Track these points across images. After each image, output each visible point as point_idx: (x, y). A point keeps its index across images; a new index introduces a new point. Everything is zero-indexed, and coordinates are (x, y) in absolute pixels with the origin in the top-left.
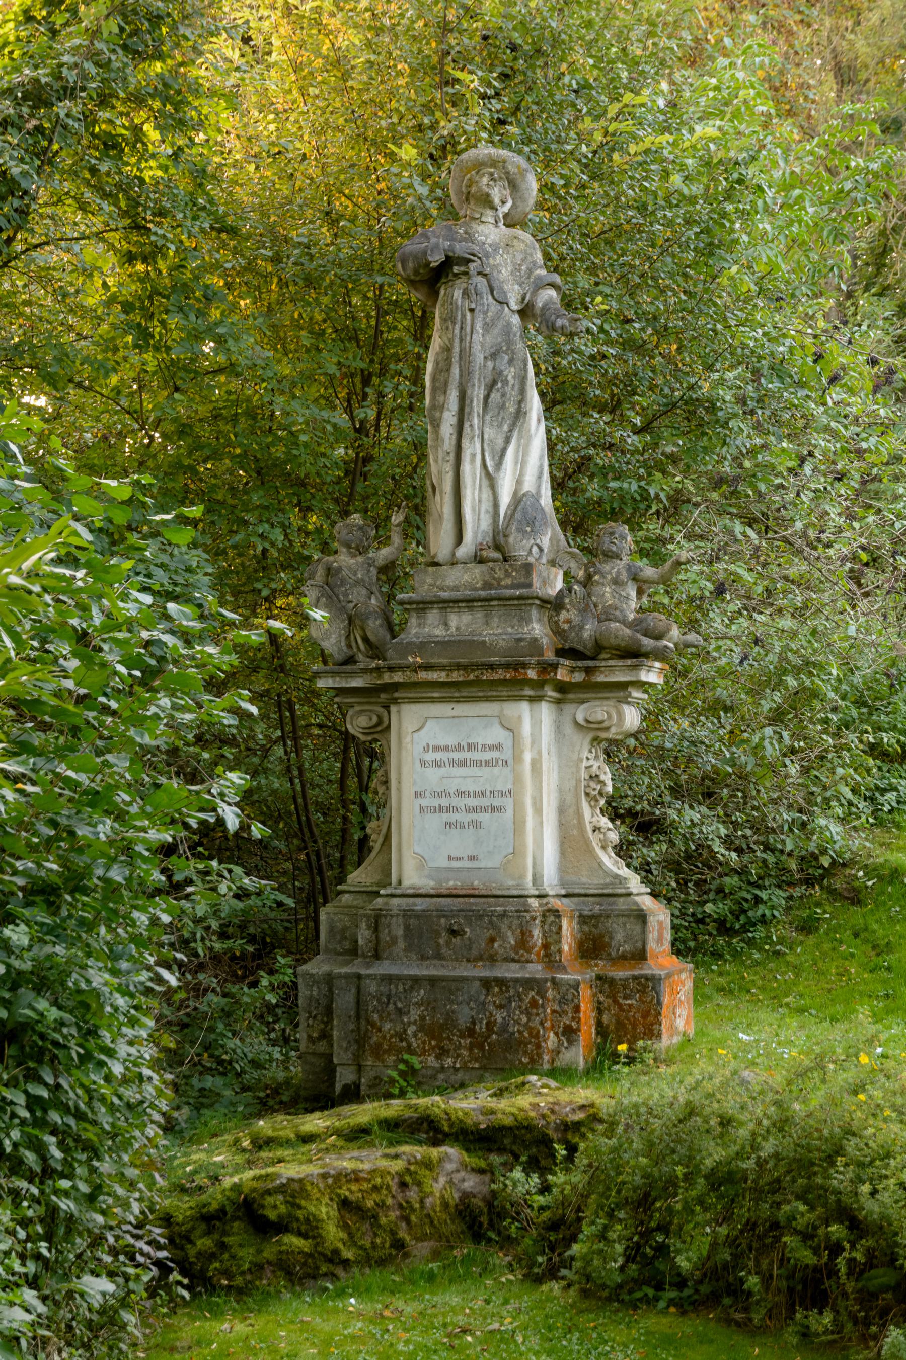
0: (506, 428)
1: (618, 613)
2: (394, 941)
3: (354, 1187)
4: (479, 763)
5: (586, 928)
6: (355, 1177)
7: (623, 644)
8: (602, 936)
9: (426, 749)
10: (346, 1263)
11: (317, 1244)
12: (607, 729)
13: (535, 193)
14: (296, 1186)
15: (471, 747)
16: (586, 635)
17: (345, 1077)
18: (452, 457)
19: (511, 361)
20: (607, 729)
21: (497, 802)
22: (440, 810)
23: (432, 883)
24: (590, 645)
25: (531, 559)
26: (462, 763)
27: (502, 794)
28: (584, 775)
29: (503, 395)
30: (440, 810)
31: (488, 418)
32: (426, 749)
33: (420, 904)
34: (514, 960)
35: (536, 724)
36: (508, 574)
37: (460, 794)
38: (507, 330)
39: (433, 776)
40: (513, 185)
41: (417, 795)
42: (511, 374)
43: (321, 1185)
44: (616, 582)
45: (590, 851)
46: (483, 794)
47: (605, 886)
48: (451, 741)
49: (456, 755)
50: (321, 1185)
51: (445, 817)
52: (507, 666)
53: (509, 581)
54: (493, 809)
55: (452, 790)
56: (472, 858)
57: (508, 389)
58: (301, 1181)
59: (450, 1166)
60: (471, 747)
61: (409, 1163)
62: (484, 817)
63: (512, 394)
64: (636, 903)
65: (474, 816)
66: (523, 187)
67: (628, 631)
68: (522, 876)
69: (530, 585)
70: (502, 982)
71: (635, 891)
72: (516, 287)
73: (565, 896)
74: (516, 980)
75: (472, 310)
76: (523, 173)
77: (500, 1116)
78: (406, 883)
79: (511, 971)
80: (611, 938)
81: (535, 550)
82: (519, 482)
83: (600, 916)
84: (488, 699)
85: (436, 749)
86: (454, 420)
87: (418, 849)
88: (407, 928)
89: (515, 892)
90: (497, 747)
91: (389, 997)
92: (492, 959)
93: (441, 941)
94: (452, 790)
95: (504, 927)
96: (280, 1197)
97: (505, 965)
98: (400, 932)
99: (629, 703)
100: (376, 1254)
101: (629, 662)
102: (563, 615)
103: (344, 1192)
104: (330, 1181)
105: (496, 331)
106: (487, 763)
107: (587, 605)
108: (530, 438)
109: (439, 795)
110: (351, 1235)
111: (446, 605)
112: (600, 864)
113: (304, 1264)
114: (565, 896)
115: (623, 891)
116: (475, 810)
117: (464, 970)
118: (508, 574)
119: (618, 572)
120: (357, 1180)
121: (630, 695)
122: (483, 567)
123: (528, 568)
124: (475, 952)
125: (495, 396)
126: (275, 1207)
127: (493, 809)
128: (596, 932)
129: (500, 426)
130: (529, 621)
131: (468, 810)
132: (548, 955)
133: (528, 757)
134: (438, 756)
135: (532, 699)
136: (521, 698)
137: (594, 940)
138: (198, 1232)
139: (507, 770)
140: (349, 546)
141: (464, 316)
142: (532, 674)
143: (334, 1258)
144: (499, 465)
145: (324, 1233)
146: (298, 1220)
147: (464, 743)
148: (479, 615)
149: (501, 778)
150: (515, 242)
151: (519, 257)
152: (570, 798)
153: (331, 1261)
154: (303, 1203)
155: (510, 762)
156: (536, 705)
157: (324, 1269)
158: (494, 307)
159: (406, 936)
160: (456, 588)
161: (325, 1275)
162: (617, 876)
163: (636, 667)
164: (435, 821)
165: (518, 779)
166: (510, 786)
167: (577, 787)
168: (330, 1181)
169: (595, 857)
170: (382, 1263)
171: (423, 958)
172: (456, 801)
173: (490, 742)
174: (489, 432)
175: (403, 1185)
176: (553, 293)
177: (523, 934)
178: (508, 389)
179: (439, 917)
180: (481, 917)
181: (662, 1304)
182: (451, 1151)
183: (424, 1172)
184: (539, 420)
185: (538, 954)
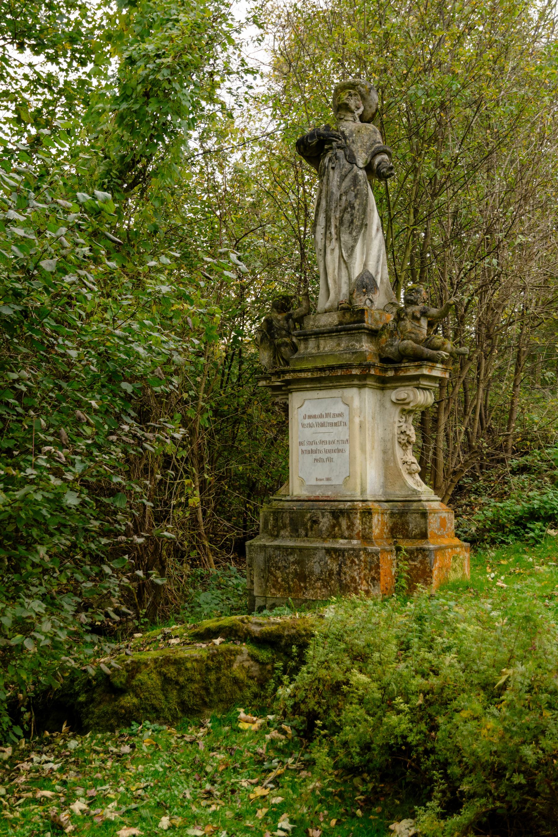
1: (413, 335)
4: (331, 425)
12: (408, 404)
15: (328, 415)
17: (259, 602)
18: (322, 253)
20: (408, 404)
22: (312, 452)
23: (310, 495)
25: (365, 307)
26: (323, 425)
27: (343, 442)
28: (396, 431)
29: (352, 215)
30: (312, 452)
32: (305, 418)
37: (322, 442)
39: (308, 432)
41: (301, 444)
45: (400, 475)
47: (408, 496)
48: (317, 413)
49: (320, 420)
51: (314, 456)
54: (339, 451)
56: (328, 479)
60: (328, 415)
62: (334, 455)
64: (423, 506)
65: (328, 455)
66: (369, 98)
68: (355, 490)
69: (364, 322)
70: (336, 550)
71: (423, 498)
75: (333, 168)
78: (295, 494)
79: (341, 543)
81: (368, 301)
82: (365, 265)
84: (335, 387)
85: (310, 417)
86: (323, 231)
90: (340, 415)
101: (416, 363)
105: (347, 180)
106: (336, 424)
109: (311, 443)
111: (318, 334)
112: (405, 483)
114: (387, 501)
115: (417, 499)
127: (339, 451)
131: (326, 452)
133: (357, 420)
134: (310, 421)
135: (361, 387)
136: (352, 386)
139: (346, 428)
141: (328, 172)
142: (355, 372)
144: (350, 255)
152: (389, 445)
155: (347, 423)
160: (325, 326)
162: (414, 490)
164: (310, 458)
165: (351, 434)
167: (393, 438)
172: (320, 447)
182: (245, 648)
184: (378, 230)
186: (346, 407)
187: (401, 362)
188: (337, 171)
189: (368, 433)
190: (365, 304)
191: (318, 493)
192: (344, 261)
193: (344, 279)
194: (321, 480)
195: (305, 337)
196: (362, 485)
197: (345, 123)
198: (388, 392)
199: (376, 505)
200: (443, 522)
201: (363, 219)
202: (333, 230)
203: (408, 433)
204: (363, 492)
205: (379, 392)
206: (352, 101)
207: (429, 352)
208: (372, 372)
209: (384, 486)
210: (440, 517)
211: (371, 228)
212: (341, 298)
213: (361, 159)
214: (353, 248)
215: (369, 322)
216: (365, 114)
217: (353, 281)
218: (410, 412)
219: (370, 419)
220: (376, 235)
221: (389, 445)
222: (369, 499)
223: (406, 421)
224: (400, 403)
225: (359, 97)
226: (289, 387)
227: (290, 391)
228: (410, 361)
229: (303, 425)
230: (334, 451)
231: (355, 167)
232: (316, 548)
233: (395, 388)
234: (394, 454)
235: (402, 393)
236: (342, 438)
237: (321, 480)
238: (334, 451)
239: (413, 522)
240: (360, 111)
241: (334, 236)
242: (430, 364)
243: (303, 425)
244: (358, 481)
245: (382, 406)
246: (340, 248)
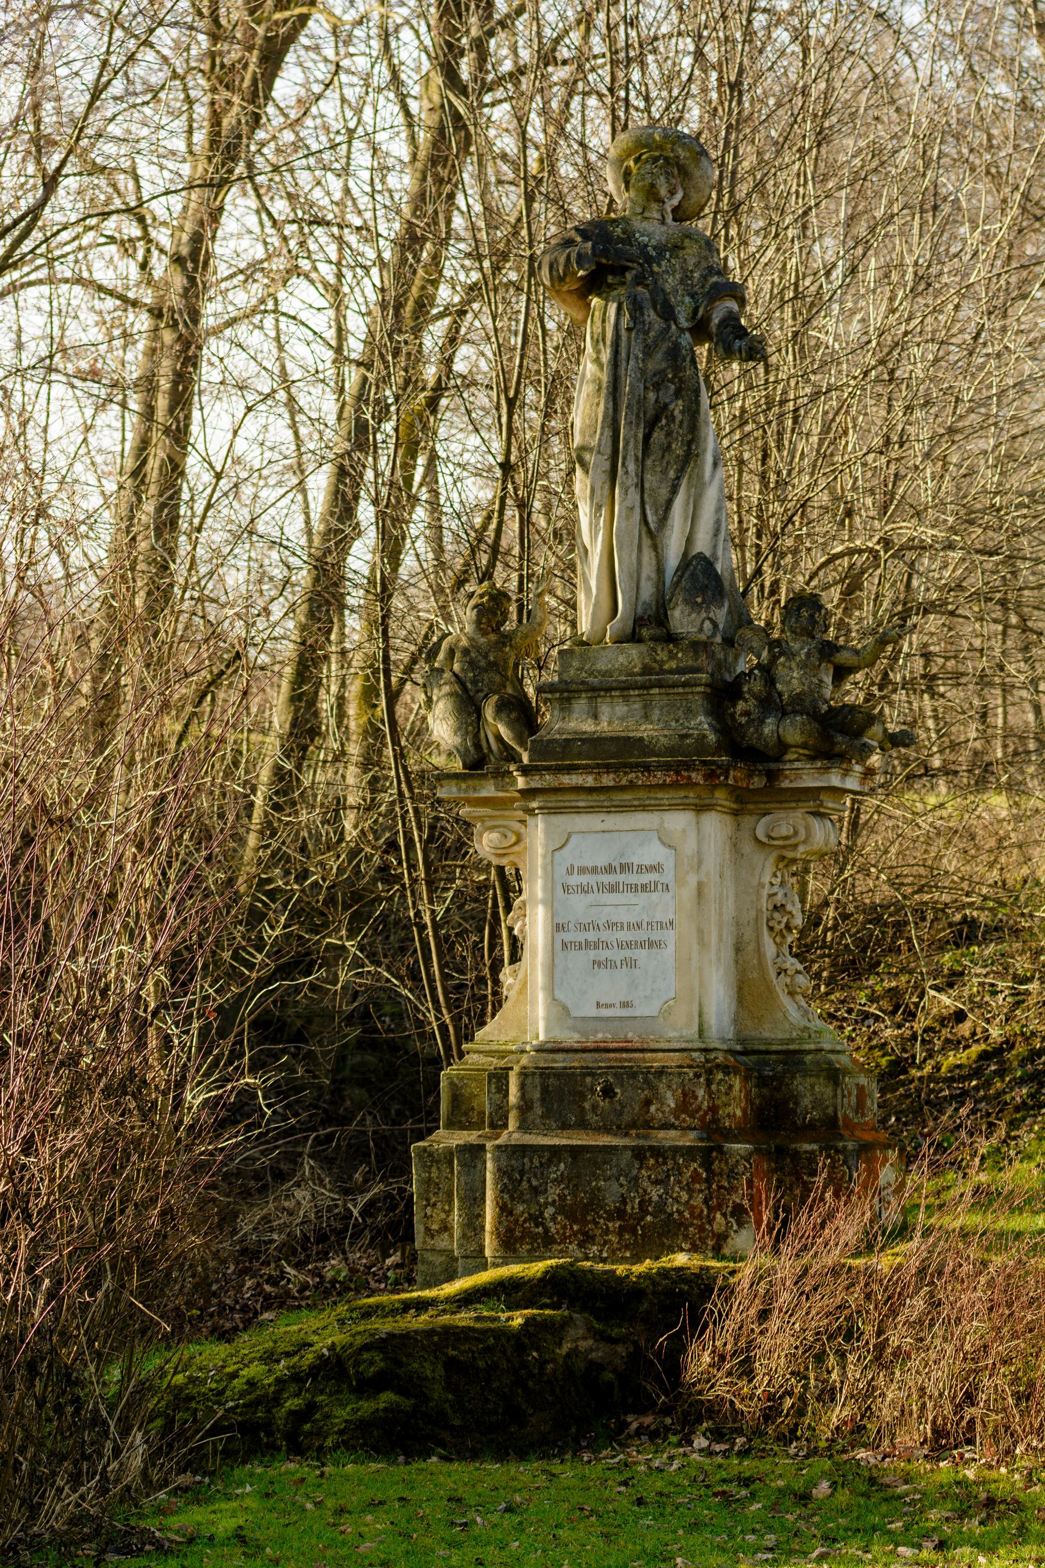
0: (672, 474)
5: (765, 1091)
9: (570, 871)
15: (625, 868)
21: (655, 936)
23: (576, 1037)
26: (613, 888)
27: (662, 926)
28: (765, 904)
29: (669, 434)
31: (649, 462)
32: (570, 871)
37: (611, 925)
42: (677, 408)
46: (639, 926)
48: (601, 862)
49: (607, 879)
51: (592, 954)
54: (651, 944)
56: (625, 1005)
57: (675, 427)
60: (625, 868)
65: (627, 953)
66: (697, 173)
80: (797, 1104)
82: (689, 541)
84: (644, 808)
85: (583, 870)
92: (648, 1125)
95: (662, 1087)
106: (644, 888)
109: (585, 928)
115: (812, 1047)
116: (629, 945)
124: (626, 1118)
125: (658, 436)
127: (651, 944)
131: (620, 946)
134: (584, 879)
139: (668, 896)
144: (664, 519)
147: (615, 864)
152: (748, 934)
159: (543, 1100)
166: (671, 917)
173: (647, 862)
178: (675, 427)
186: (667, 851)
190: (701, 630)
192: (649, 531)
193: (648, 569)
194: (608, 1006)
201: (689, 444)
205: (728, 818)
209: (736, 1021)
211: (703, 463)
214: (669, 503)
216: (685, 205)
221: (748, 934)
229: (566, 888)
234: (759, 950)
236: (658, 917)
237: (608, 1006)
240: (675, 202)
243: (566, 888)
245: (735, 846)
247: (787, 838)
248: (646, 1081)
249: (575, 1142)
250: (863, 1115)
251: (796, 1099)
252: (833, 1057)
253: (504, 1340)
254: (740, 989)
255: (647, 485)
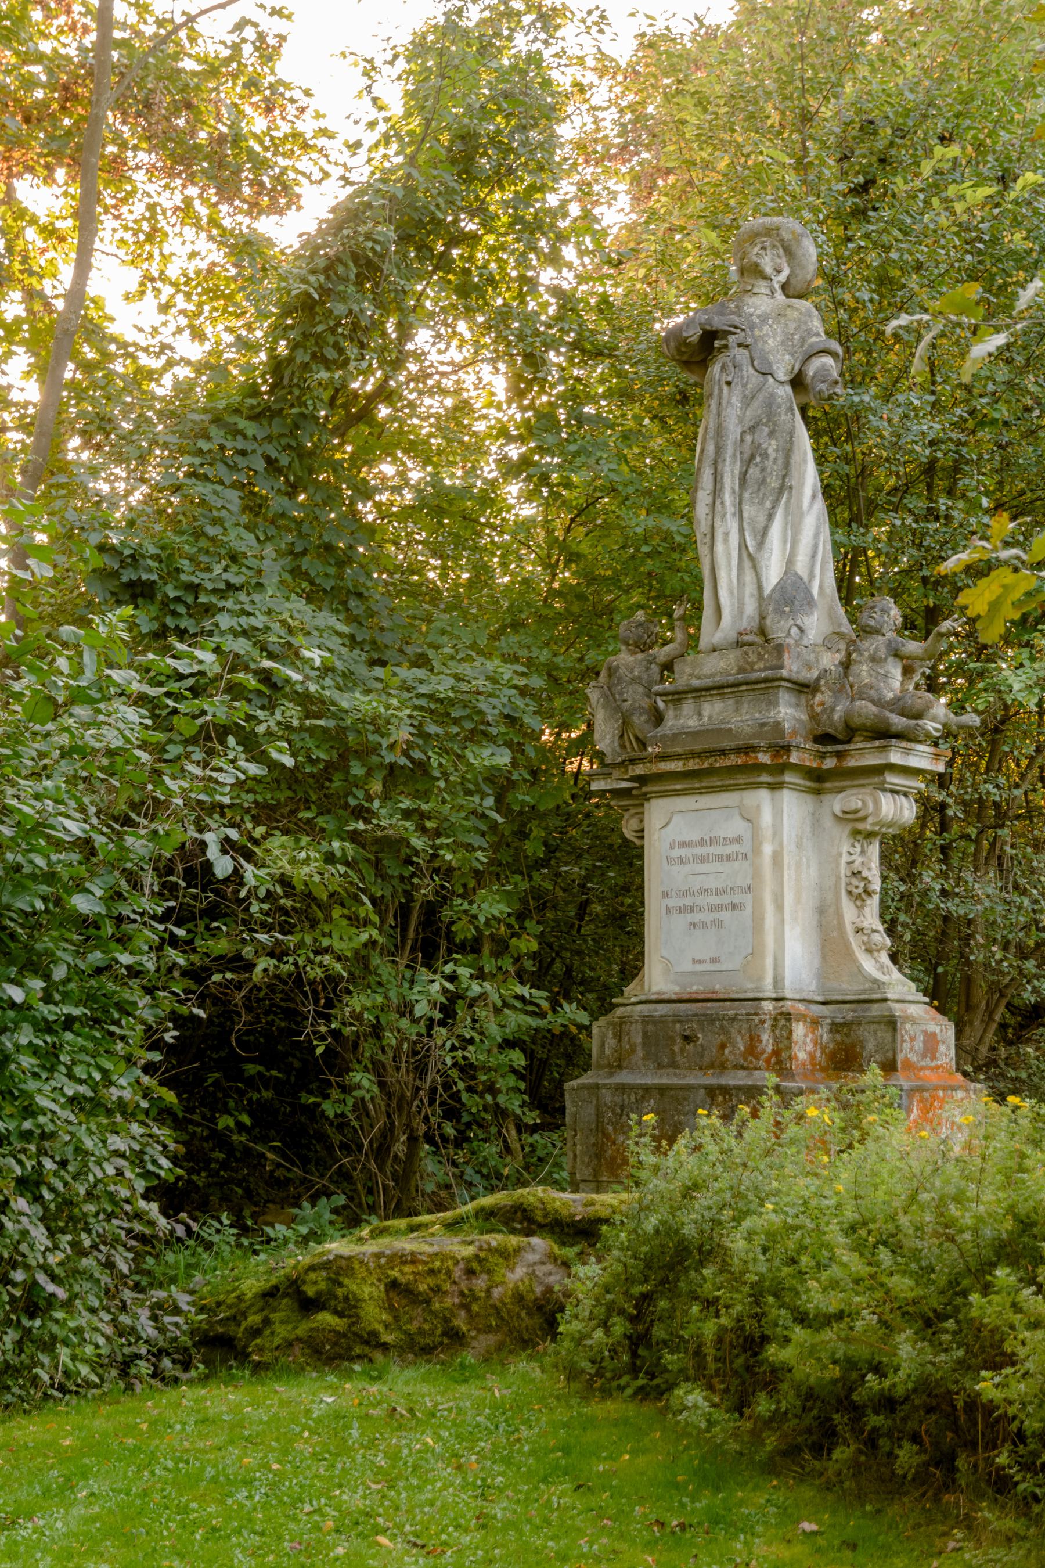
0: (768, 504)
1: (872, 692)
2: (633, 1051)
3: (407, 1269)
5: (838, 1037)
6: (413, 1259)
7: (868, 723)
8: (854, 1046)
9: (672, 847)
10: (385, 1347)
11: (353, 1324)
12: (864, 819)
13: (814, 258)
14: (343, 1263)
15: (713, 841)
16: (836, 716)
18: (708, 540)
19: (772, 434)
21: (737, 899)
22: (685, 909)
23: (677, 989)
24: (840, 727)
26: (705, 859)
27: (741, 890)
28: (843, 870)
29: (763, 470)
30: (685, 909)
31: (746, 495)
32: (672, 847)
33: (661, 1009)
34: (743, 1068)
35: (778, 813)
36: (760, 658)
37: (704, 891)
38: (770, 404)
39: (679, 872)
40: (789, 253)
41: (665, 895)
42: (772, 447)
43: (372, 1265)
44: (873, 659)
45: (849, 954)
46: (725, 891)
47: (864, 992)
48: (695, 837)
49: (700, 851)
50: (372, 1265)
51: (689, 917)
52: (738, 750)
53: (761, 665)
54: (734, 907)
55: (696, 888)
56: (714, 960)
57: (769, 463)
58: (349, 1258)
59: (531, 1257)
60: (713, 841)
61: (481, 1249)
62: (725, 916)
63: (774, 468)
65: (715, 915)
67: (874, 709)
68: (761, 978)
69: (782, 667)
70: (725, 1090)
72: (787, 357)
73: (824, 1003)
74: (739, 1088)
75: (729, 383)
76: (798, 238)
77: (597, 1207)
80: (863, 1048)
81: (794, 631)
82: (790, 562)
83: (851, 1023)
84: (727, 788)
85: (682, 845)
86: (709, 500)
87: (665, 953)
88: (645, 1035)
89: (750, 995)
90: (737, 840)
91: (622, 1107)
92: (723, 1067)
93: (676, 1048)
94: (696, 888)
95: (734, 1032)
96: (324, 1274)
97: (733, 1073)
98: (638, 1040)
99: (884, 790)
100: (422, 1341)
101: (877, 743)
102: (819, 698)
103: (395, 1273)
104: (383, 1261)
105: (756, 404)
106: (729, 858)
107: (843, 686)
108: (801, 515)
110: (396, 1318)
111: (700, 693)
112: (860, 969)
113: (335, 1344)
114: (824, 1003)
116: (717, 908)
117: (691, 1080)
118: (760, 658)
119: (877, 649)
120: (413, 1262)
121: (884, 782)
122: (738, 652)
123: (779, 649)
124: (707, 1060)
125: (754, 472)
126: (315, 1283)
127: (734, 907)
128: (848, 1041)
129: (761, 503)
130: (776, 704)
132: (779, 1062)
133: (768, 849)
136: (758, 785)
137: (846, 1050)
138: (254, 1309)
139: (746, 864)
140: (627, 644)
141: (721, 390)
142: (764, 758)
143: (372, 1341)
144: (761, 544)
145: (362, 1314)
146: (336, 1297)
147: (707, 838)
148: (731, 702)
149: (737, 873)
150: (789, 311)
151: (792, 326)
153: (367, 1343)
154: (346, 1281)
156: (777, 794)
157: (358, 1350)
158: (755, 379)
159: (644, 1044)
160: (713, 675)
161: (359, 1357)
162: (876, 981)
163: (884, 748)
164: (680, 921)
165: (757, 874)
166: (749, 881)
168: (383, 1261)
169: (855, 961)
170: (427, 1351)
171: (660, 1066)
173: (730, 835)
174: (748, 510)
175: (470, 1272)
176: (829, 361)
177: (751, 1038)
178: (769, 463)
179: (674, 1022)
180: (712, 1021)
181: (629, 1391)
183: (494, 1259)
184: (814, 497)
185: (768, 1061)
186: (746, 824)
187: (849, 741)
188: (737, 389)
189: (788, 874)
190: (789, 634)
191: (696, 988)
192: (750, 555)
193: (750, 589)
194: (701, 962)
195: (677, 697)
196: (775, 969)
197: (755, 299)
198: (827, 798)
199: (801, 1007)
200: (931, 1043)
202: (728, 497)
203: (865, 873)
204: (778, 981)
205: (809, 798)
206: (767, 259)
207: (898, 722)
208: (794, 758)
209: (822, 975)
210: (925, 1032)
211: (801, 494)
212: (744, 624)
213: (783, 366)
214: (766, 530)
215: (792, 667)
216: (793, 281)
217: (767, 590)
218: (870, 835)
219: (793, 847)
220: (811, 506)
222: (788, 995)
223: (863, 852)
224: (850, 819)
225: (781, 252)
226: (644, 789)
227: (646, 797)
228: (867, 739)
230: (724, 907)
231: (771, 380)
232: (689, 1088)
233: (840, 791)
234: (839, 916)
235: (852, 799)
237: (701, 962)
238: (724, 907)
239: (871, 1040)
240: (783, 277)
241: (730, 509)
242: (904, 744)
243: (670, 861)
244: (769, 962)
245: (816, 821)
246: (742, 531)
247: (856, 811)
248: (722, 1027)
249: (665, 1080)
250: (933, 1058)
251: (862, 1043)
252: (897, 1006)
253: (450, 1263)
254: (823, 947)
255: (745, 515)
